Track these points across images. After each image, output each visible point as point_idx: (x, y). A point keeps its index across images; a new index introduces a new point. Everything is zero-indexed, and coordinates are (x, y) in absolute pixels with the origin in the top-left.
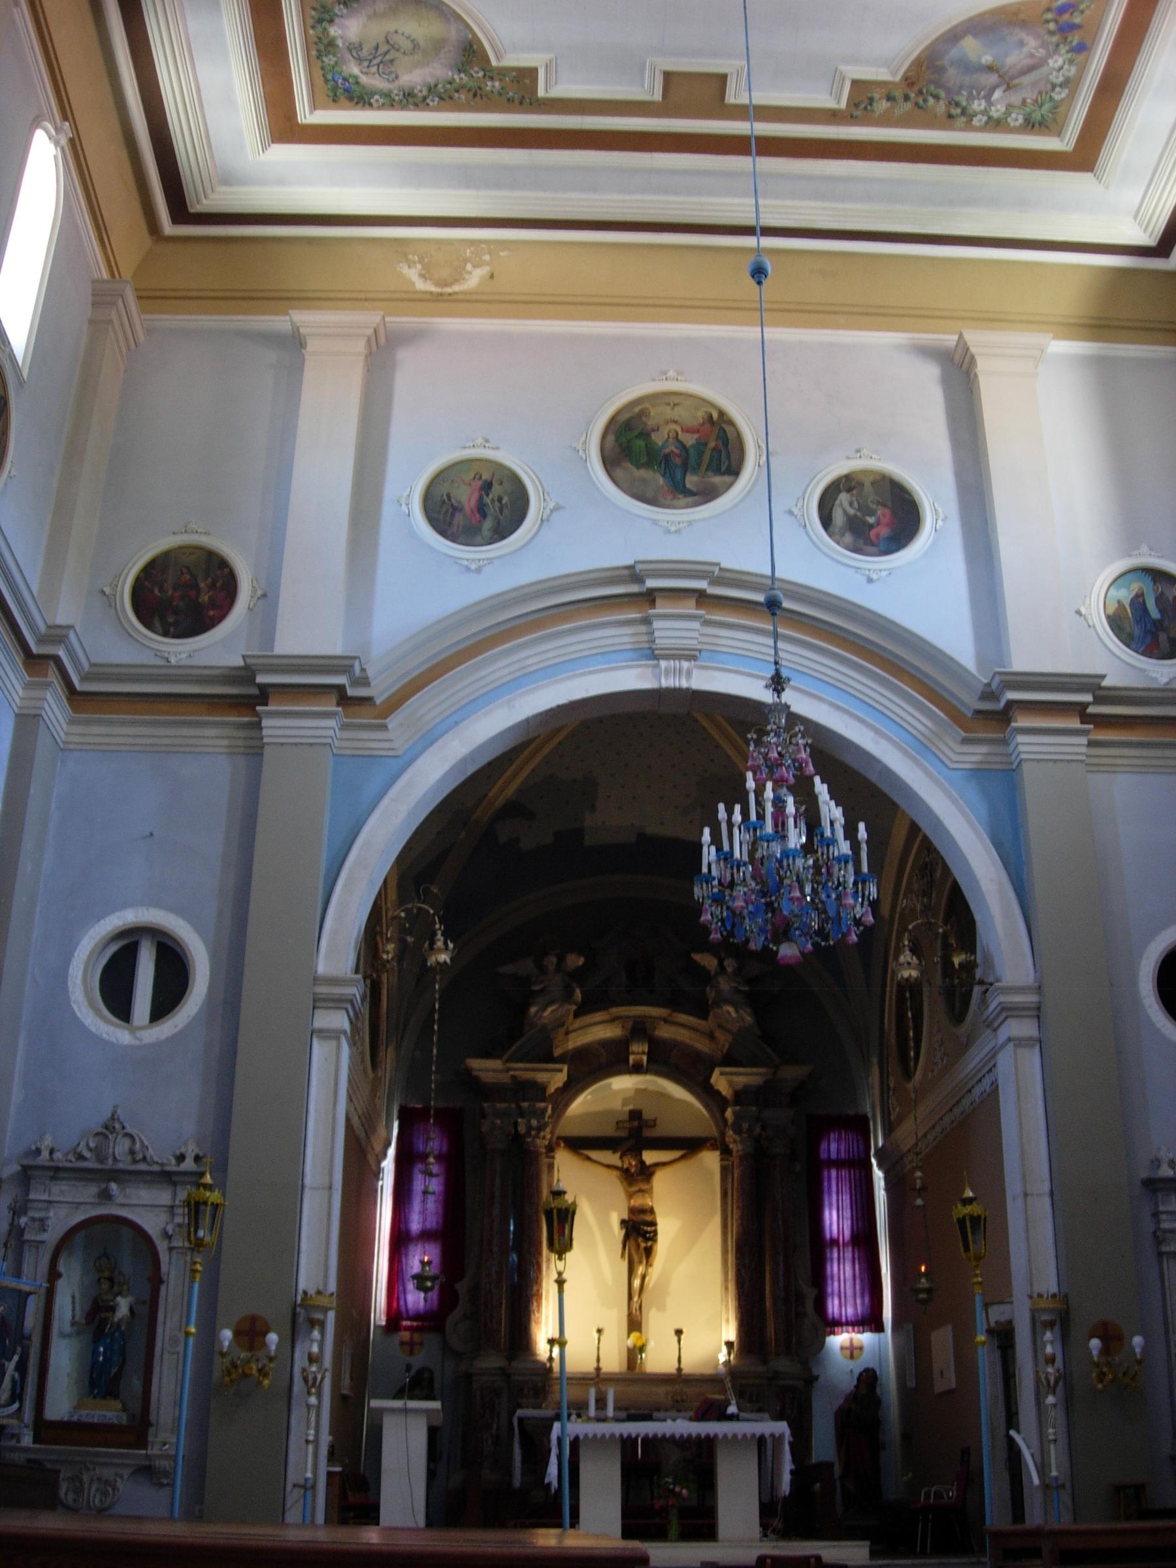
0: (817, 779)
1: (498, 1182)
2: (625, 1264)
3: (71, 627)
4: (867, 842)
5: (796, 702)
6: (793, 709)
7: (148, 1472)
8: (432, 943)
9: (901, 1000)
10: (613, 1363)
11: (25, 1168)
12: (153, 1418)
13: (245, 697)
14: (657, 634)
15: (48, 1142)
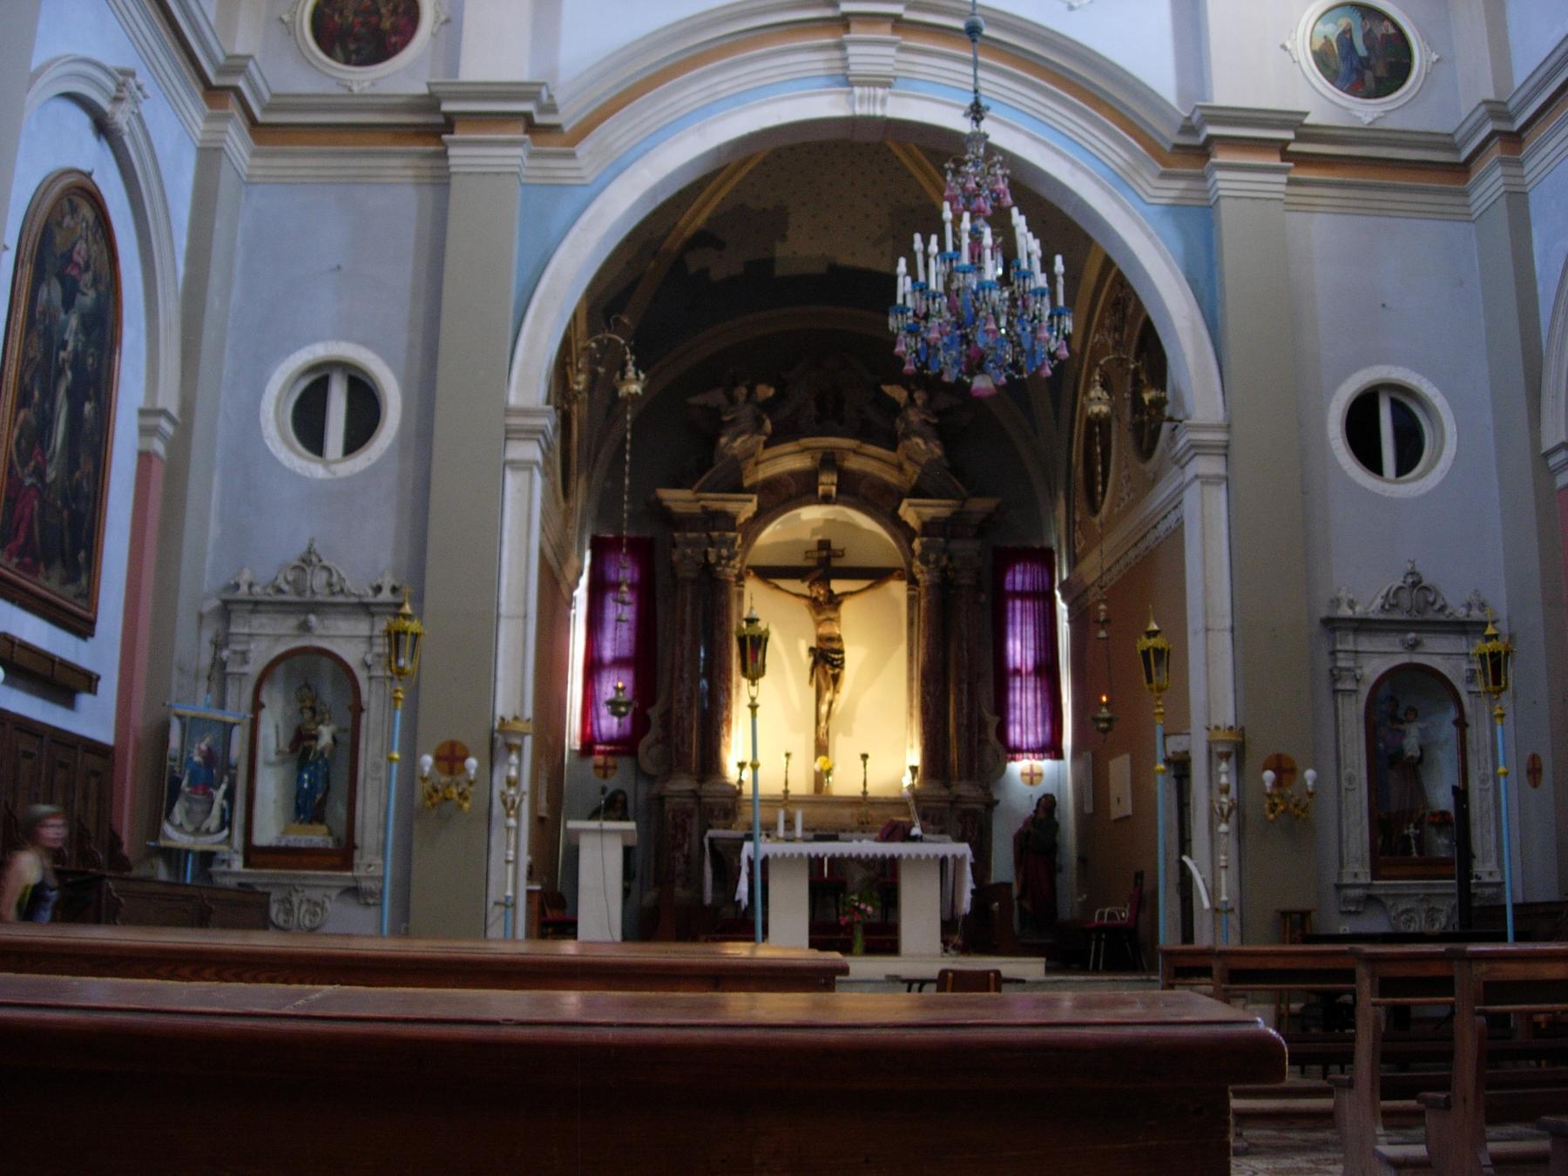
0: (1015, 211)
1: (688, 608)
2: (812, 691)
3: (249, 57)
4: (1064, 276)
5: (998, 134)
6: (993, 140)
7: (353, 892)
8: (623, 374)
9: (1089, 436)
10: (801, 785)
11: (226, 603)
12: (358, 841)
13: (431, 125)
14: (851, 60)
15: (246, 576)
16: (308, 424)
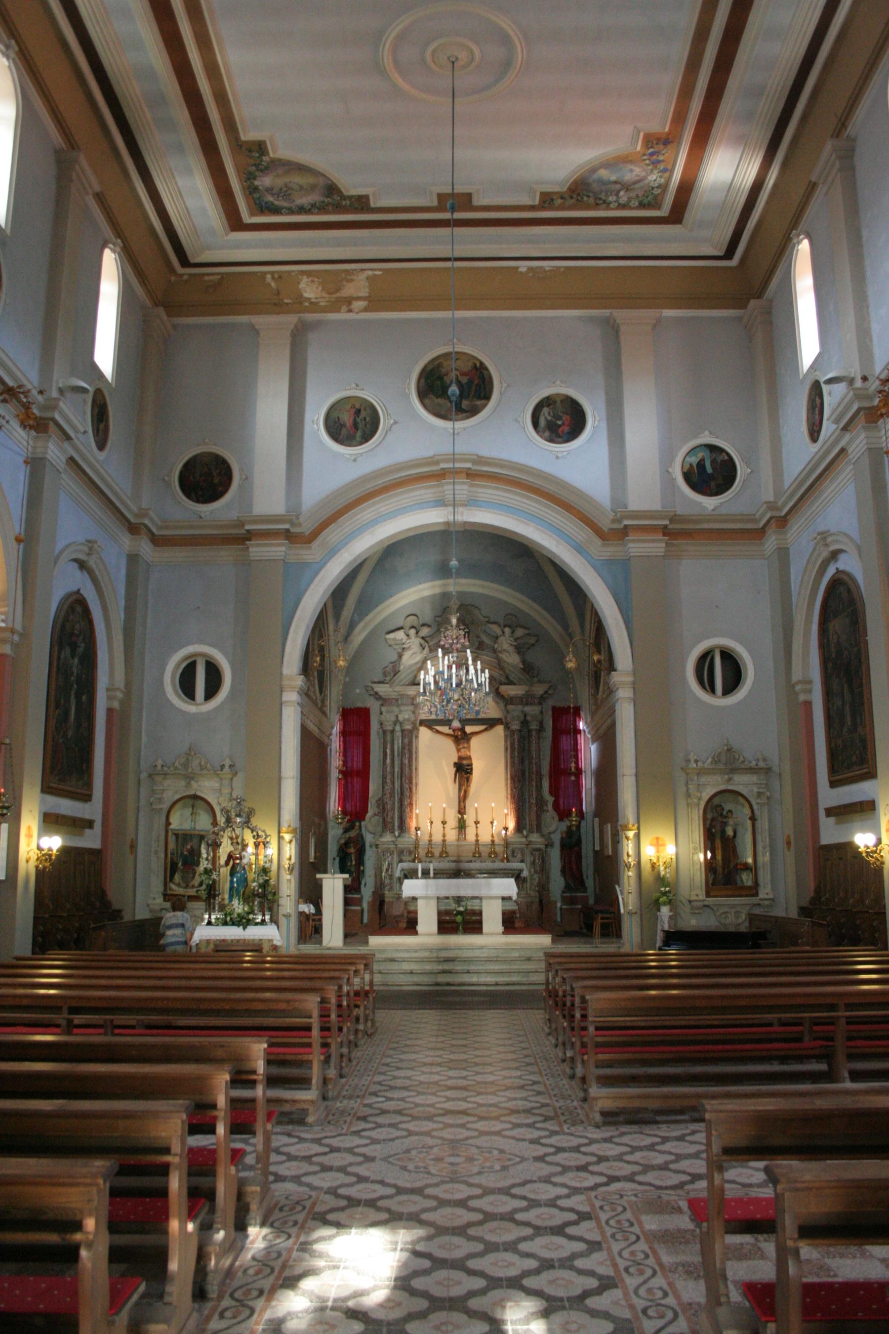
16: (187, 686)
